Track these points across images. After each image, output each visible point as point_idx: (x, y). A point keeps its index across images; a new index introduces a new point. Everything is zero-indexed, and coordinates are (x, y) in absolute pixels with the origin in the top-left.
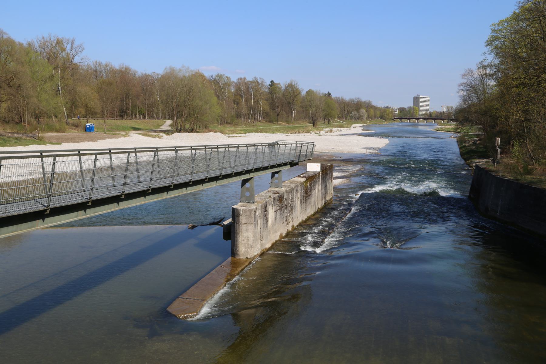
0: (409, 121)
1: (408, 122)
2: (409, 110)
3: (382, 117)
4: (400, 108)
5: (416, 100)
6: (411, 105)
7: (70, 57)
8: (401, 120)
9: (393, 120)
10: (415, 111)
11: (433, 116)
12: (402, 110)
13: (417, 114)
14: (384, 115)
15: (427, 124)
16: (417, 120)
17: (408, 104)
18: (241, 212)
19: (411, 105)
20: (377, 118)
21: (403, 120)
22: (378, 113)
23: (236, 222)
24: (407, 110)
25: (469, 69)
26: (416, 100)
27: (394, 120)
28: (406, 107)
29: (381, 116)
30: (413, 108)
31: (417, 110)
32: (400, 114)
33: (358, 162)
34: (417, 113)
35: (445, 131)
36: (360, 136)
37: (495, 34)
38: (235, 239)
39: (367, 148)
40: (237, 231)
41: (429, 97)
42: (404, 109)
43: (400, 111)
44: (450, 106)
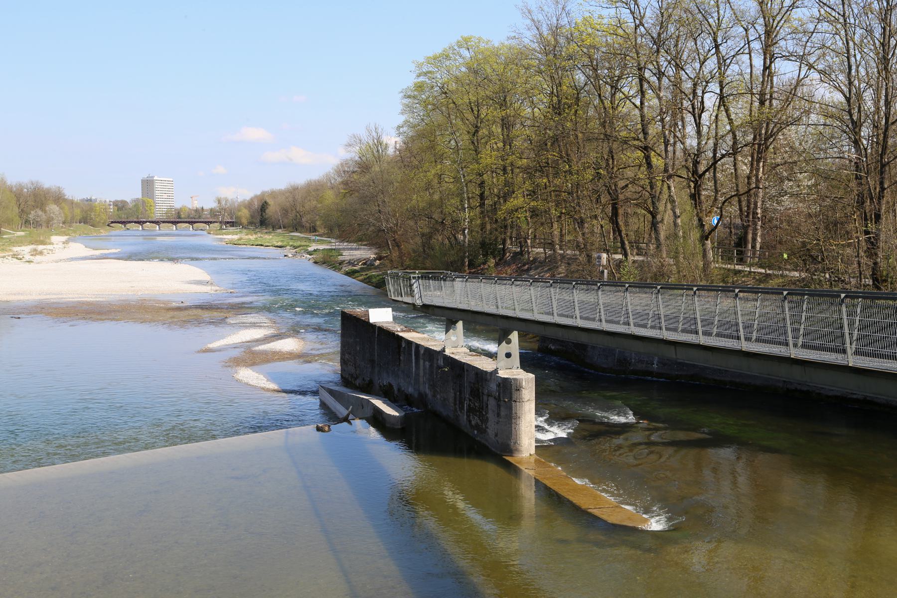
0: (142, 227)
1: (141, 228)
2: (135, 206)
3: (85, 220)
4: (117, 201)
5: (148, 185)
6: (139, 195)
7: (654, 82)
8: (125, 226)
9: (108, 225)
10: (147, 206)
11: (182, 216)
12: (120, 206)
13: (151, 213)
14: (91, 215)
15: (160, 232)
16: (142, 225)
17: (131, 193)
18: (524, 383)
19: (139, 195)
20: (76, 223)
21: (128, 226)
22: (77, 211)
23: (513, 399)
24: (131, 205)
25: (354, 135)
26: (148, 185)
27: (112, 225)
28: (128, 200)
29: (83, 218)
30: (144, 202)
31: (151, 206)
32: (116, 212)
33: (100, 313)
34: (152, 211)
35: (253, 245)
36: (122, 259)
37: (421, 79)
38: (511, 427)
39: (190, 283)
40: (516, 413)
41: (172, 180)
42: (124, 203)
43: (116, 208)
44: (222, 197)
